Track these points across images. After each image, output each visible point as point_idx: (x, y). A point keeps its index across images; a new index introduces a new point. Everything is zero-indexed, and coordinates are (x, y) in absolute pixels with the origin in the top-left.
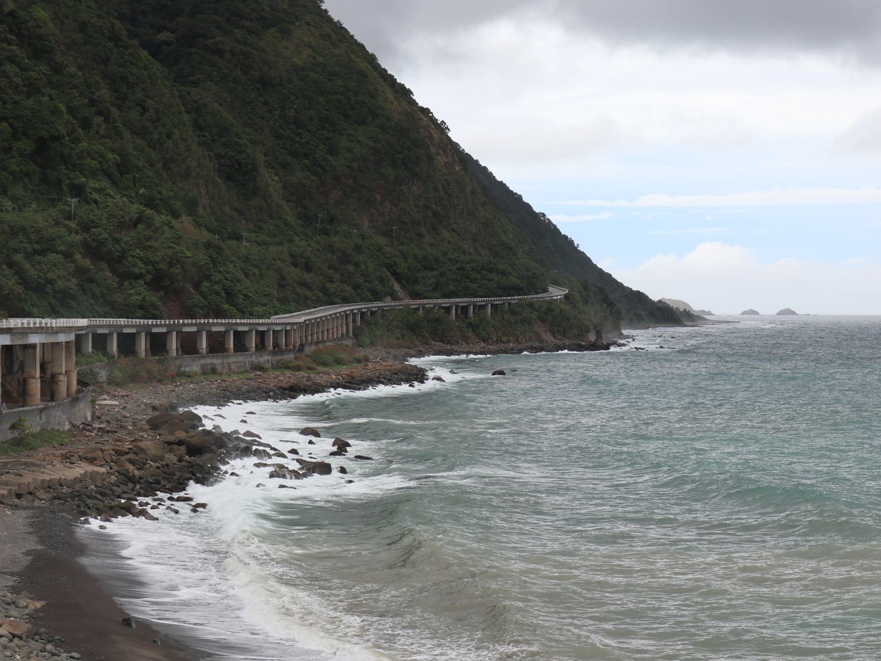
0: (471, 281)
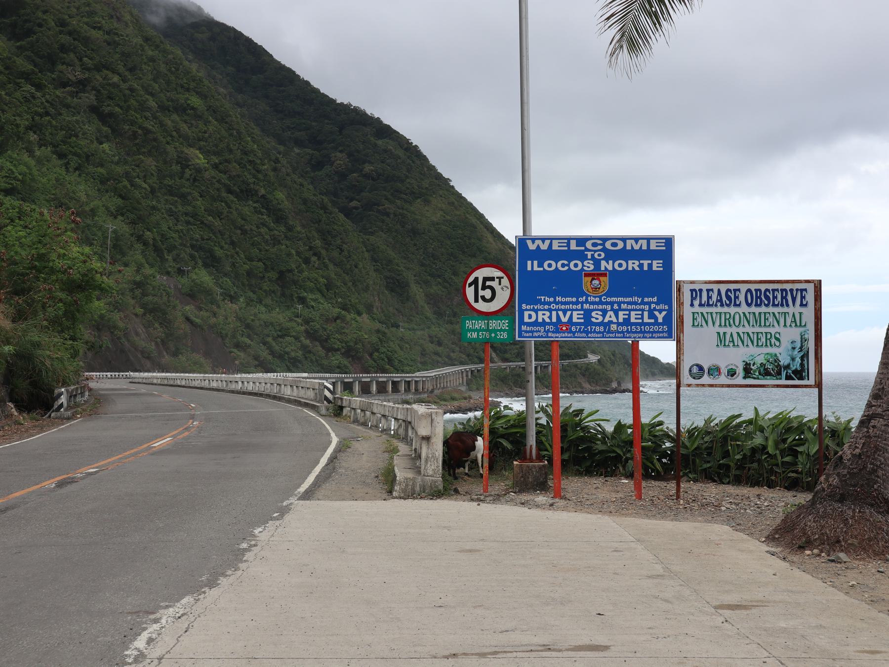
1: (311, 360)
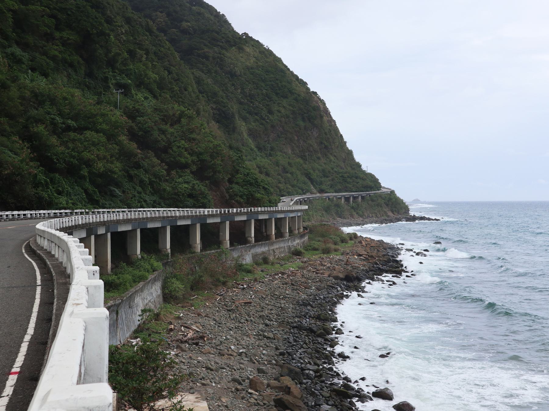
0: (348, 183)
1: (142, 182)
